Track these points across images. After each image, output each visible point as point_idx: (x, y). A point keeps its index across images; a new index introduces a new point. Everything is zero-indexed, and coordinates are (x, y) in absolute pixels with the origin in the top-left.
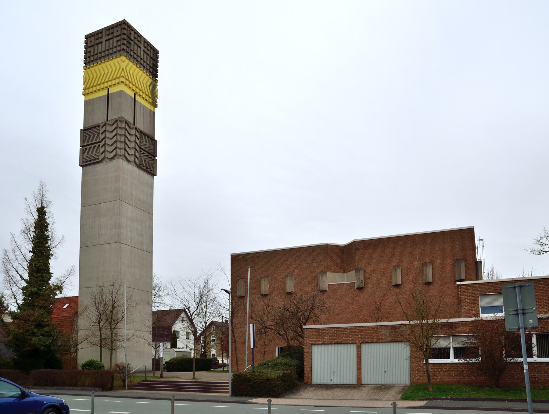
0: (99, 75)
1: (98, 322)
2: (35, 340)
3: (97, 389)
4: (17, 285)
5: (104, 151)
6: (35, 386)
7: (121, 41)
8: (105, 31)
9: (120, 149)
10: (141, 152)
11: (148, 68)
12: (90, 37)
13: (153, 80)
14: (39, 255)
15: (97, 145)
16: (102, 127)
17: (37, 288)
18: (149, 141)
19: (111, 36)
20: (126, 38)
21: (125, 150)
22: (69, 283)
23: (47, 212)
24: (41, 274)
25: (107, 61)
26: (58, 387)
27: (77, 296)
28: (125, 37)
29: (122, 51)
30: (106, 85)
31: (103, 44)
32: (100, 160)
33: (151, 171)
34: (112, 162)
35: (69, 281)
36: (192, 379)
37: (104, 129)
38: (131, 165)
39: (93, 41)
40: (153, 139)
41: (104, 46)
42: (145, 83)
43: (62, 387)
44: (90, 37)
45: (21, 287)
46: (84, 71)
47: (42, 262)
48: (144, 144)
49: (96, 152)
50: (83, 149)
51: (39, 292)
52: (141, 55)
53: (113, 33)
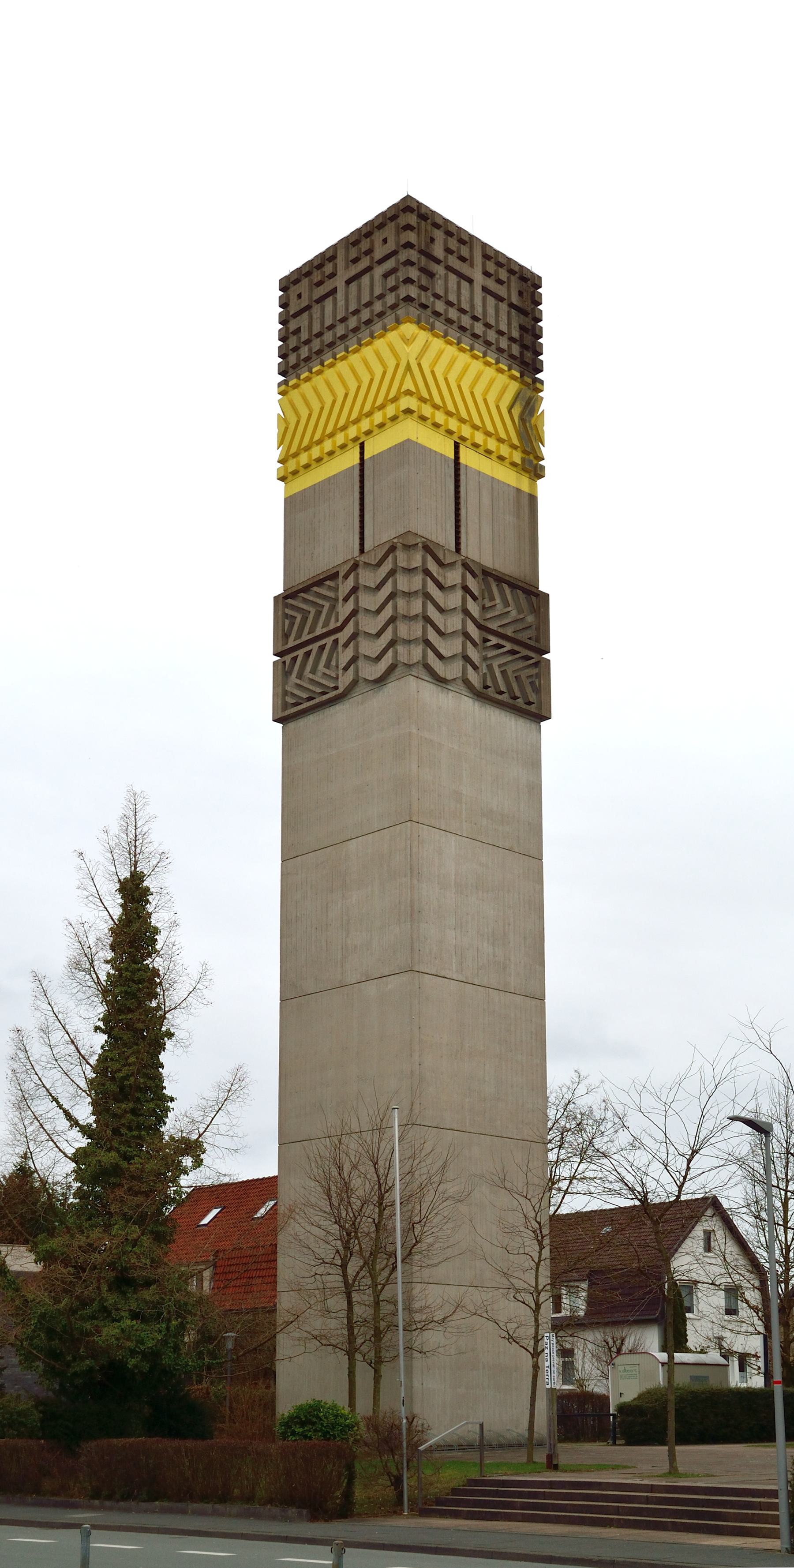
0: (328, 400)
1: (339, 1262)
2: (110, 1332)
3: (292, 1511)
4: (57, 1147)
5: (354, 660)
6: (93, 1497)
7: (399, 274)
8: (343, 250)
9: (408, 642)
10: (489, 644)
11: (504, 343)
12: (296, 282)
13: (523, 382)
14: (125, 1038)
15: (329, 641)
16: (346, 577)
17: (118, 1151)
18: (516, 599)
19: (365, 263)
20: (414, 259)
21: (427, 643)
22: (223, 1129)
23: (152, 890)
24: (131, 1105)
25: (356, 351)
26: (166, 1504)
27: (275, 1177)
28: (413, 255)
29: (402, 304)
30: (352, 432)
31: (340, 295)
32: (341, 690)
33: (530, 703)
34: (381, 693)
35: (226, 1120)
36: (664, 1476)
37: (350, 582)
38: (451, 694)
39: (307, 293)
40: (533, 590)
41: (341, 303)
42: (491, 399)
43: (179, 1505)
44: (296, 282)
45: (70, 1151)
46: (279, 401)
47: (134, 1064)
48: (497, 613)
49: (328, 665)
50: (284, 663)
51: (124, 1164)
52: (472, 306)
53: (369, 252)
